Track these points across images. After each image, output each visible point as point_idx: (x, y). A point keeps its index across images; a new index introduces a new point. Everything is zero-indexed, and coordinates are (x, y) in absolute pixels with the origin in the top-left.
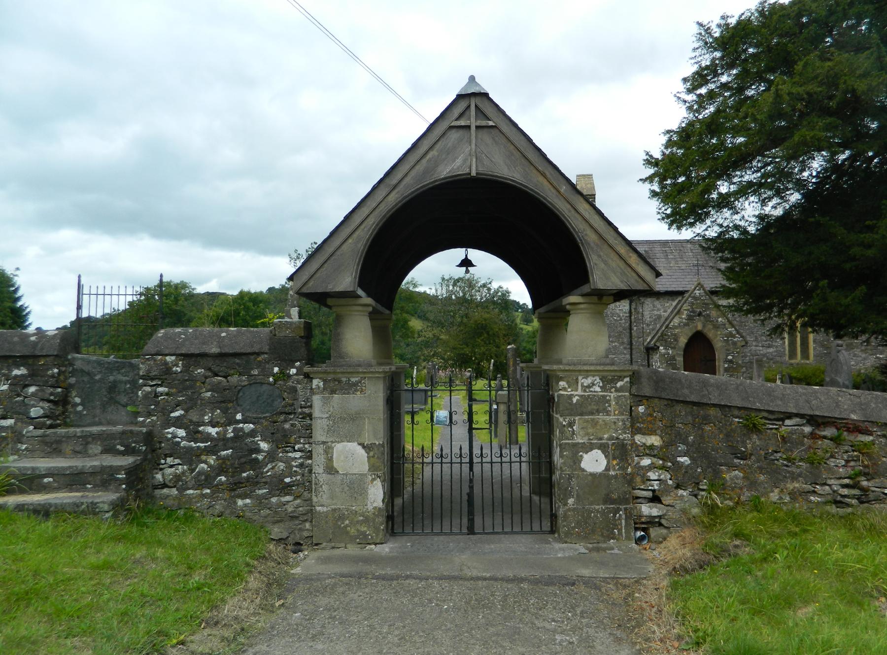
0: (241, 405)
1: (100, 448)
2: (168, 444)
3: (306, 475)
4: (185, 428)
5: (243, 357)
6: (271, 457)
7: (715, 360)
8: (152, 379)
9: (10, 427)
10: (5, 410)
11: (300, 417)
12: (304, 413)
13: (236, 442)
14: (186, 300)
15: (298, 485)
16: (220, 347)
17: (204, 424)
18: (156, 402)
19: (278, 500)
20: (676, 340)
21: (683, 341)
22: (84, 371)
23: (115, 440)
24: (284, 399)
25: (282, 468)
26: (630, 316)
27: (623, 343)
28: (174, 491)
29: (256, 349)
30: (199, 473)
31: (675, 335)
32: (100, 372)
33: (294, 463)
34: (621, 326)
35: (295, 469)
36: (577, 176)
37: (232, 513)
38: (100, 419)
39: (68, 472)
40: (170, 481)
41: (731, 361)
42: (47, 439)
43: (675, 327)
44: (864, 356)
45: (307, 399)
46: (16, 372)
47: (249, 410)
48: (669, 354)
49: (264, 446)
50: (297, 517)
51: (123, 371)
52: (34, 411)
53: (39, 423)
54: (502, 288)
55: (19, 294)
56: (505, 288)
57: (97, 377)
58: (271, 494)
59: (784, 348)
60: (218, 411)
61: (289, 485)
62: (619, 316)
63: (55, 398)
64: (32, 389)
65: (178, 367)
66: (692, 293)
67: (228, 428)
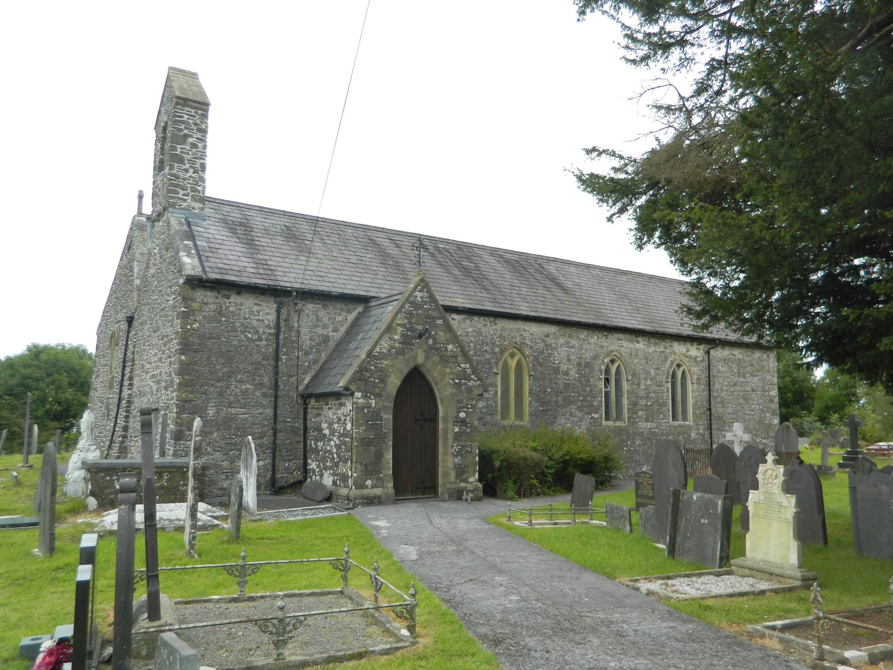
7: (434, 420)
20: (383, 381)
21: (394, 382)
26: (277, 335)
27: (261, 385)
31: (382, 370)
34: (259, 352)
36: (170, 68)
41: (463, 422)
43: (382, 356)
44: (579, 415)
48: (370, 407)
59: (496, 402)
62: (257, 332)
66: (410, 295)
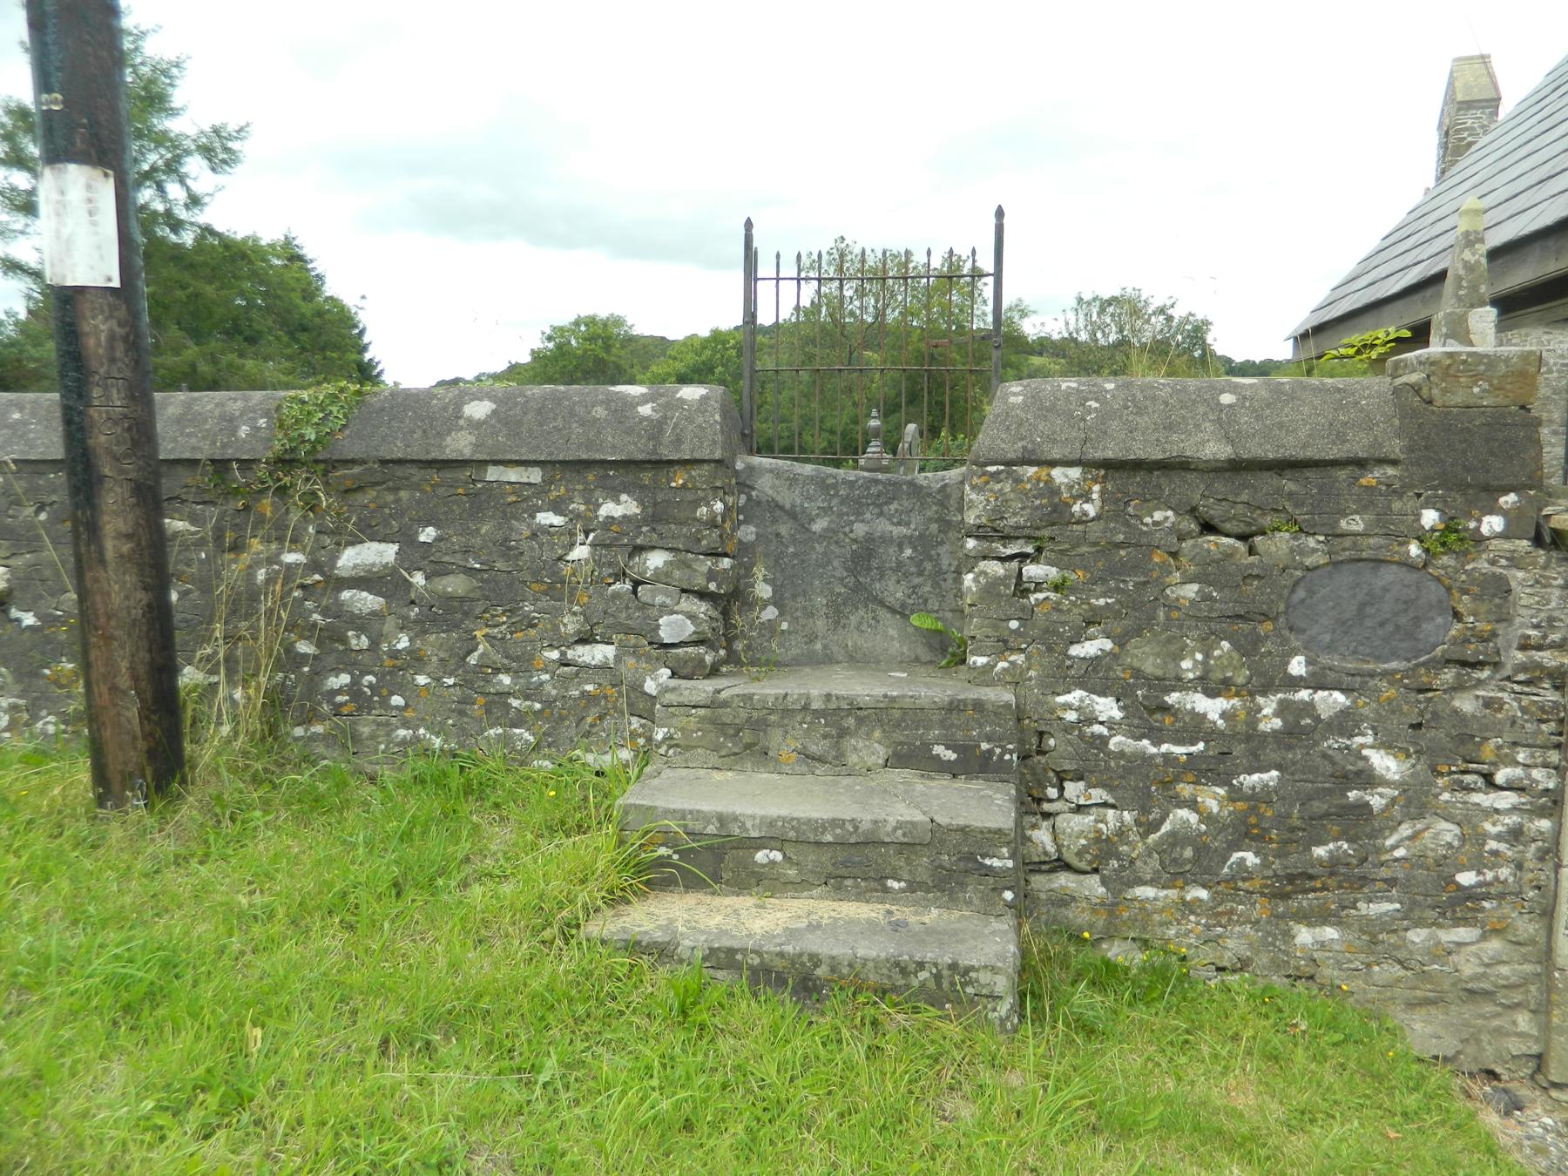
0: (1304, 631)
1: (881, 752)
2: (1070, 742)
3: (1529, 865)
4: (1121, 695)
5: (1311, 474)
6: (1415, 801)
8: (1006, 538)
9: (603, 668)
10: (587, 620)
11: (1521, 677)
12: (1539, 666)
13: (1290, 748)
14: (623, 347)
15: (1501, 896)
16: (1229, 440)
17: (1179, 684)
18: (1023, 608)
19: (1431, 937)
22: (782, 508)
23: (928, 728)
24: (1457, 616)
25: (1448, 838)
28: (1094, 887)
29: (1358, 445)
30: (1175, 839)
32: (826, 511)
33: (1488, 826)
34: (1548, 385)
35: (1492, 845)
37: (1276, 965)
38: (825, 647)
39: (829, 838)
40: (1079, 854)
42: (726, 715)
45: (1551, 620)
46: (609, 509)
47: (1330, 648)
49: (1385, 763)
50: (1488, 995)
51: (894, 506)
52: (669, 624)
53: (686, 661)
54: (1193, 315)
55: (366, 339)
56: (1200, 317)
57: (818, 526)
58: (1411, 916)
60: (1225, 645)
61: (1470, 896)
63: (719, 587)
64: (656, 560)
65: (1088, 500)
67: (1260, 700)
